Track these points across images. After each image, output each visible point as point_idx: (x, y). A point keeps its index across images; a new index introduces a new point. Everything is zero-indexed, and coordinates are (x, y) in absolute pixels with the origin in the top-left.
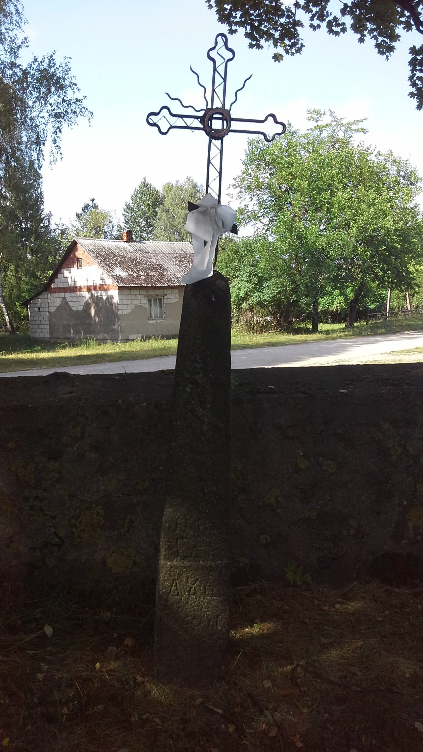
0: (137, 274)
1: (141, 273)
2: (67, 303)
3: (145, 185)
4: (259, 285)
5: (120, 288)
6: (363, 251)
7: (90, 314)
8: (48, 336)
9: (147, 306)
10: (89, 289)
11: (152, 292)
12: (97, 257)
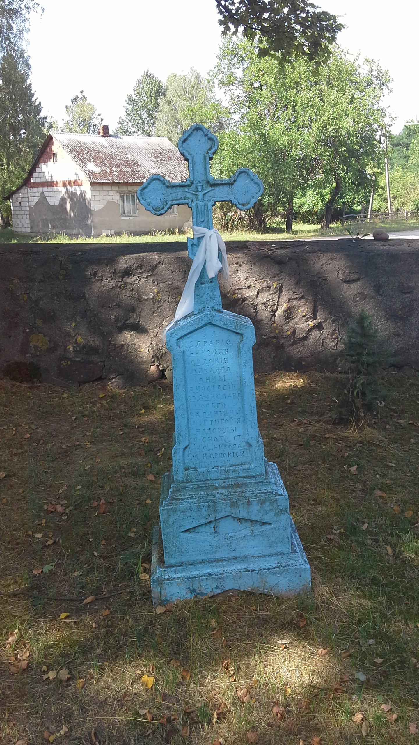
0: (110, 169)
1: (114, 169)
2: (45, 198)
3: (148, 75)
5: (92, 184)
6: (322, 152)
7: (66, 209)
8: (29, 230)
9: (119, 202)
10: (64, 185)
11: (125, 188)
12: (71, 152)
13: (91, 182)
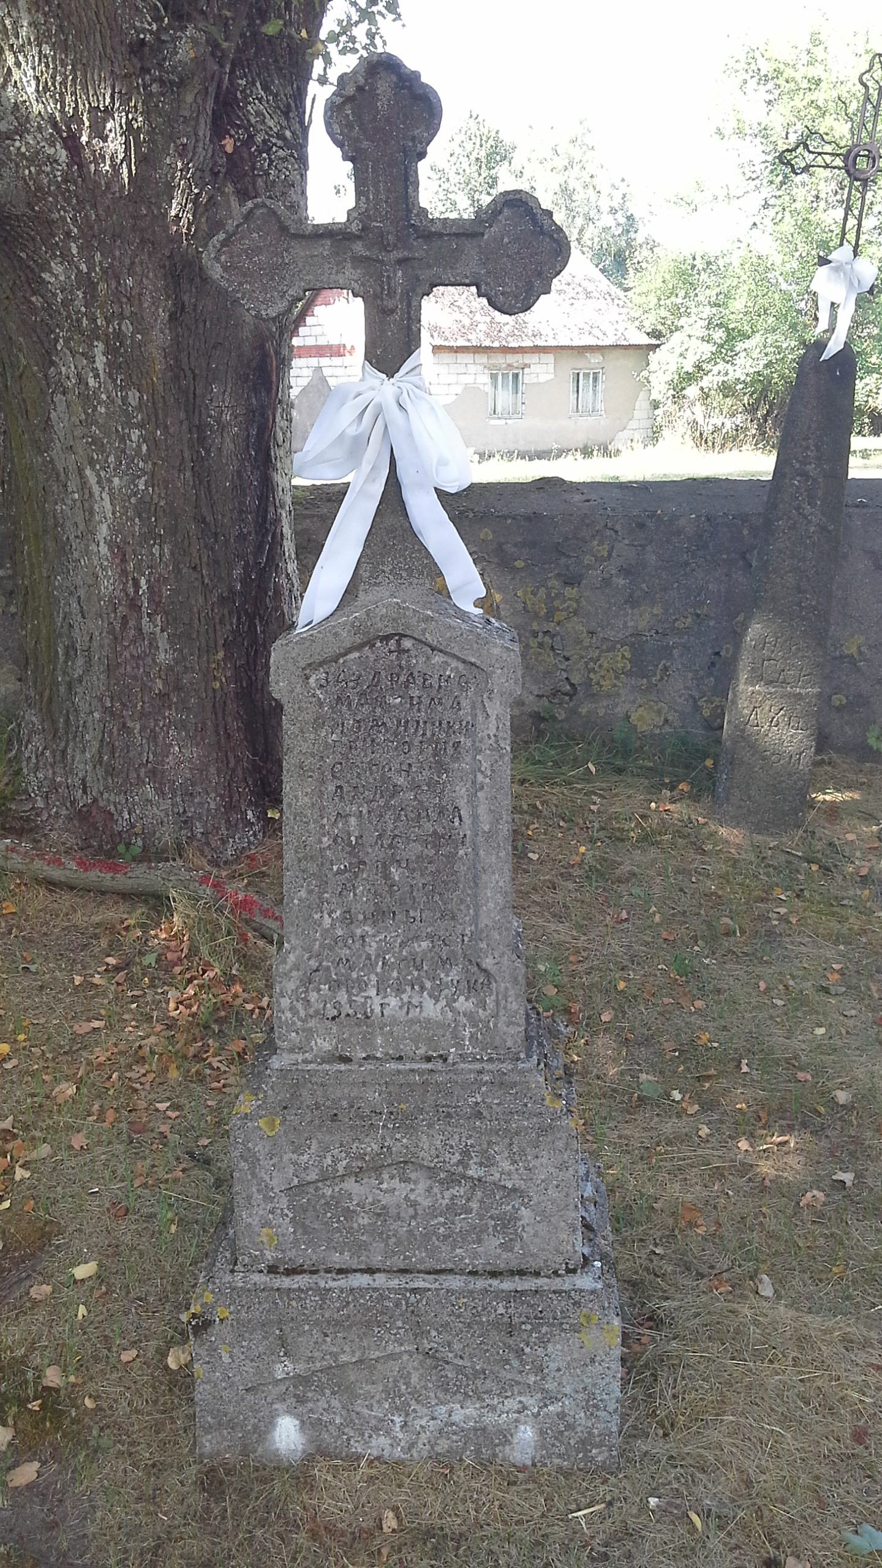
2: (324, 380)
4: (726, 351)
9: (489, 388)
11: (500, 360)
13: (434, 347)
